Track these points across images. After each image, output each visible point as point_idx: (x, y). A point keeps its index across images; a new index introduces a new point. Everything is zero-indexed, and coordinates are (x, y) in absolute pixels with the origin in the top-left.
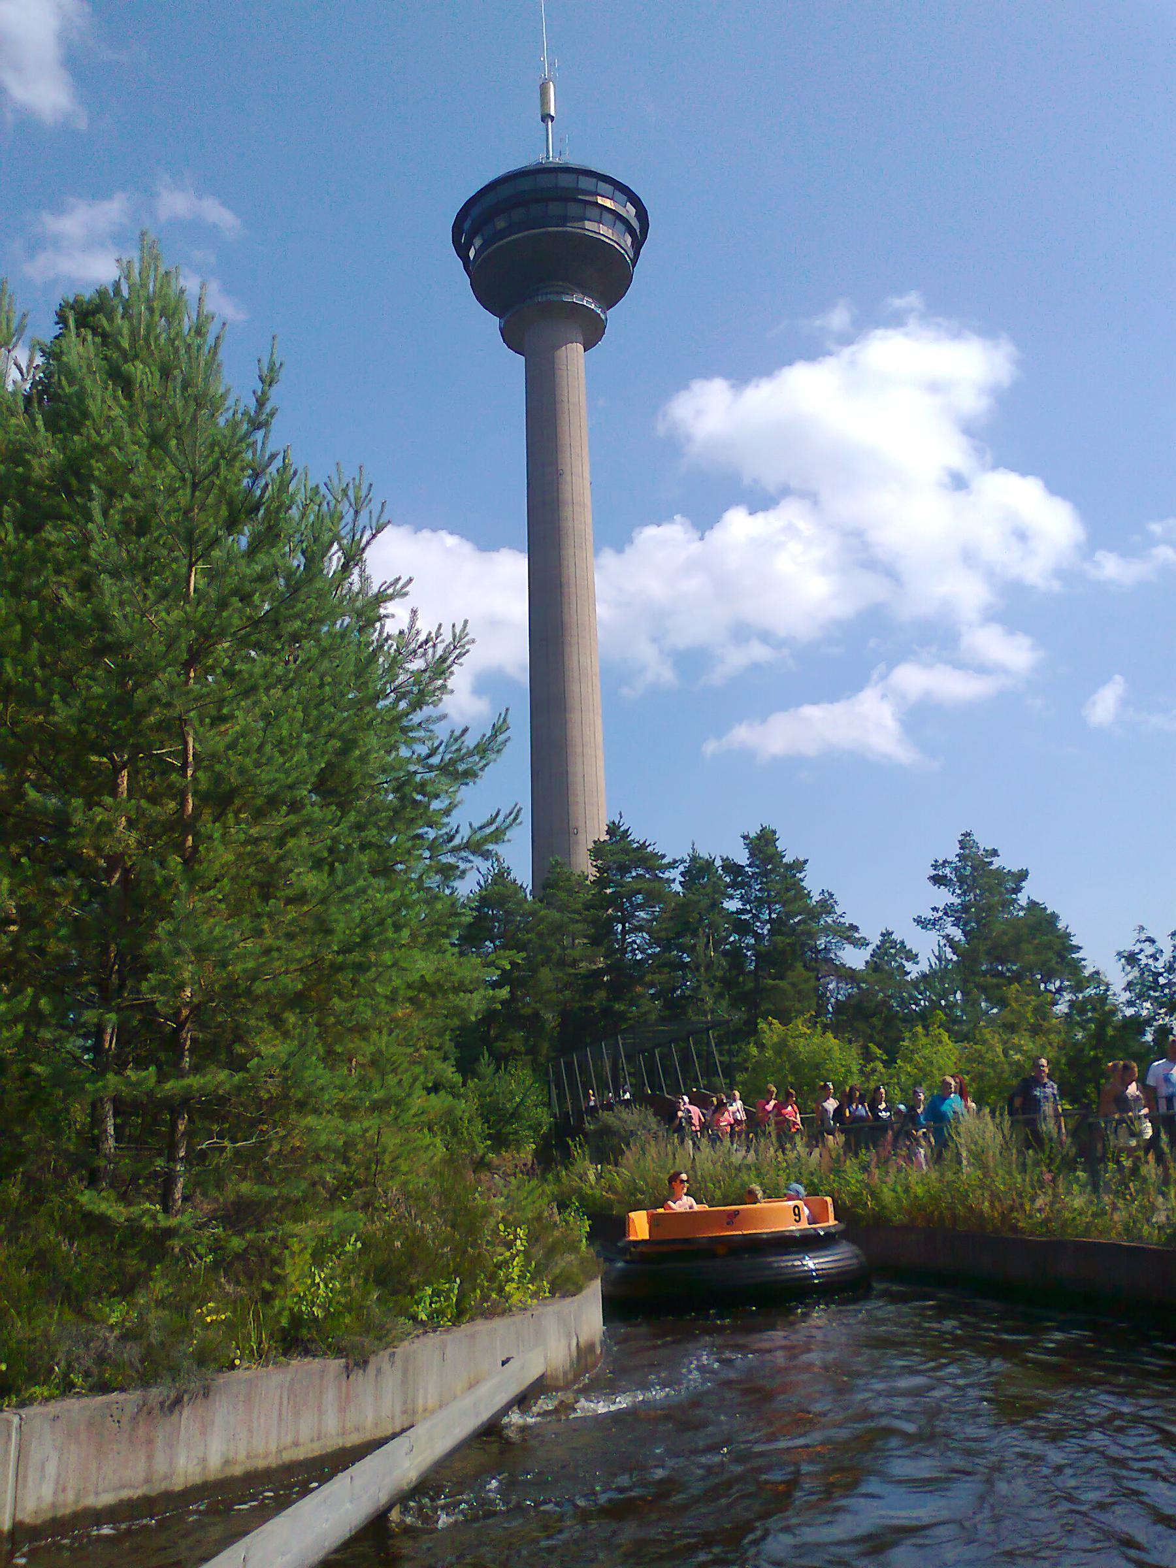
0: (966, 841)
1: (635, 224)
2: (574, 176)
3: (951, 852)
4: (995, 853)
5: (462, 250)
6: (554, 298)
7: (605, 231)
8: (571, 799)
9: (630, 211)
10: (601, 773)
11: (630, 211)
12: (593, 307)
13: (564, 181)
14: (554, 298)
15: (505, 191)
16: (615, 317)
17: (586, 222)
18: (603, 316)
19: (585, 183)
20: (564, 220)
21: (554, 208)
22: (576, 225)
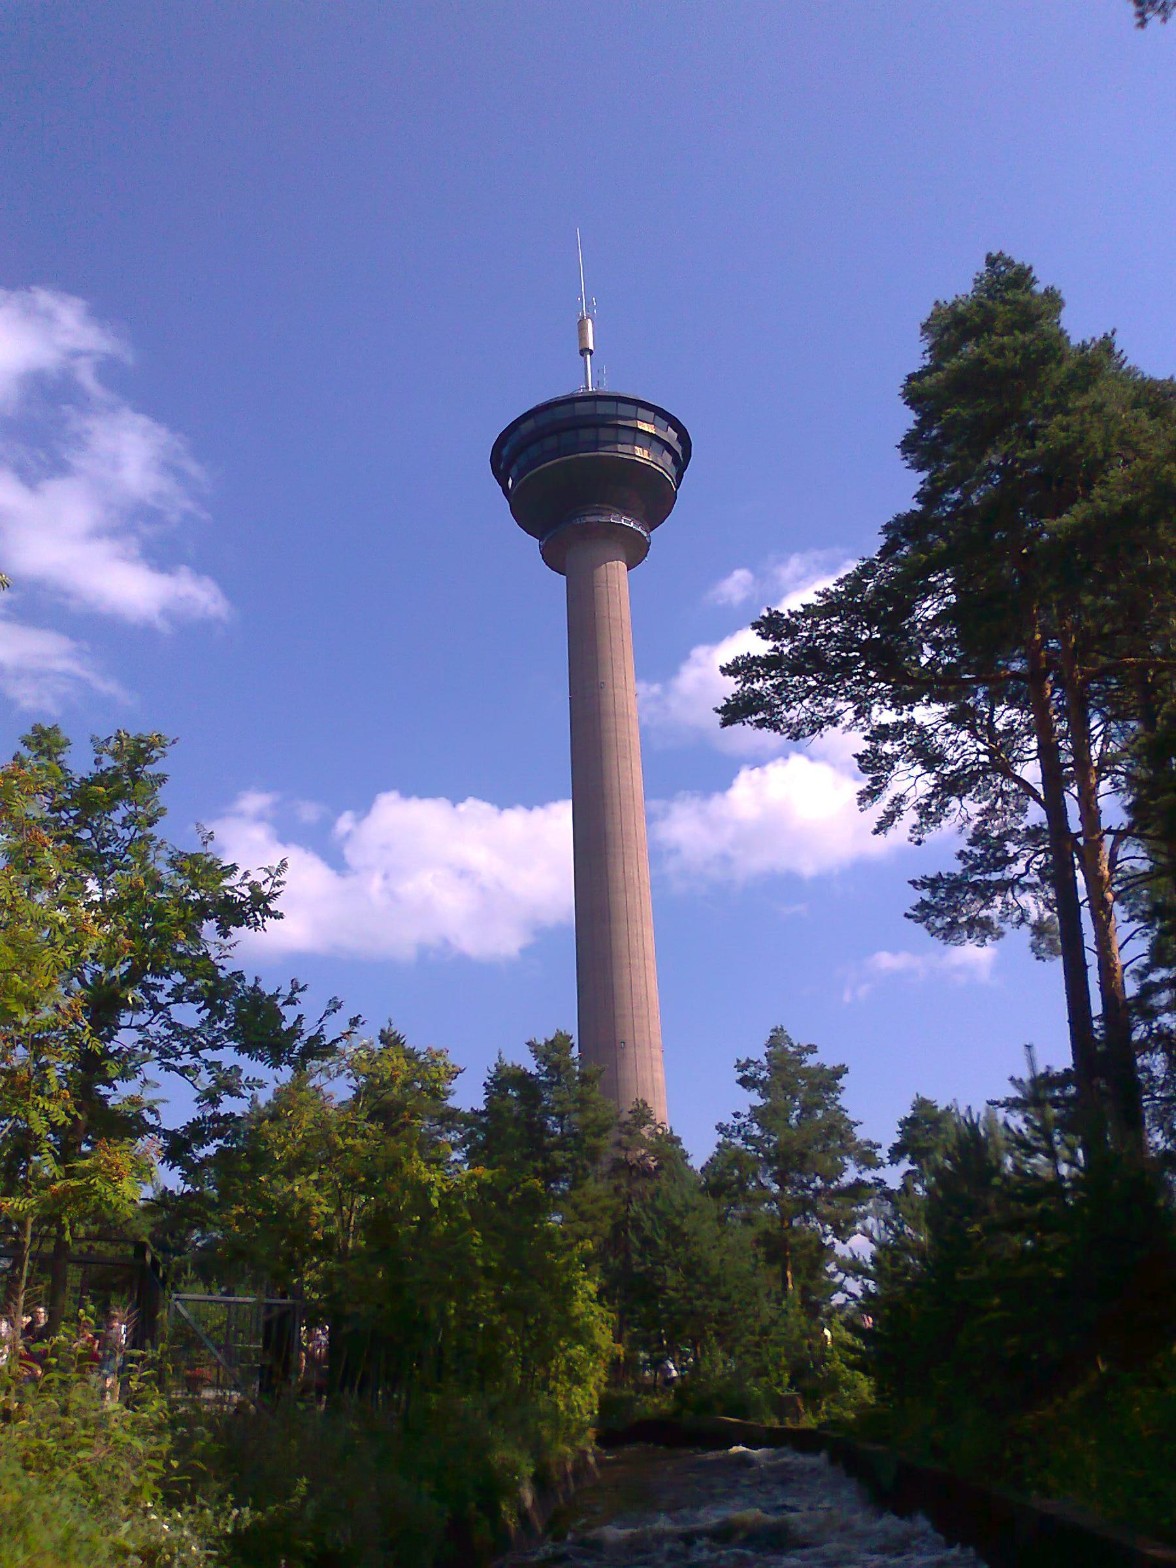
0: (777, 1038)
1: (678, 448)
2: (590, 404)
3: (758, 1052)
4: (812, 1049)
5: (501, 479)
8: (617, 1012)
9: (671, 435)
10: (653, 985)
11: (671, 435)
12: (632, 525)
13: (603, 408)
16: (657, 536)
19: (624, 409)
20: (596, 445)
21: (586, 435)
22: (608, 448)
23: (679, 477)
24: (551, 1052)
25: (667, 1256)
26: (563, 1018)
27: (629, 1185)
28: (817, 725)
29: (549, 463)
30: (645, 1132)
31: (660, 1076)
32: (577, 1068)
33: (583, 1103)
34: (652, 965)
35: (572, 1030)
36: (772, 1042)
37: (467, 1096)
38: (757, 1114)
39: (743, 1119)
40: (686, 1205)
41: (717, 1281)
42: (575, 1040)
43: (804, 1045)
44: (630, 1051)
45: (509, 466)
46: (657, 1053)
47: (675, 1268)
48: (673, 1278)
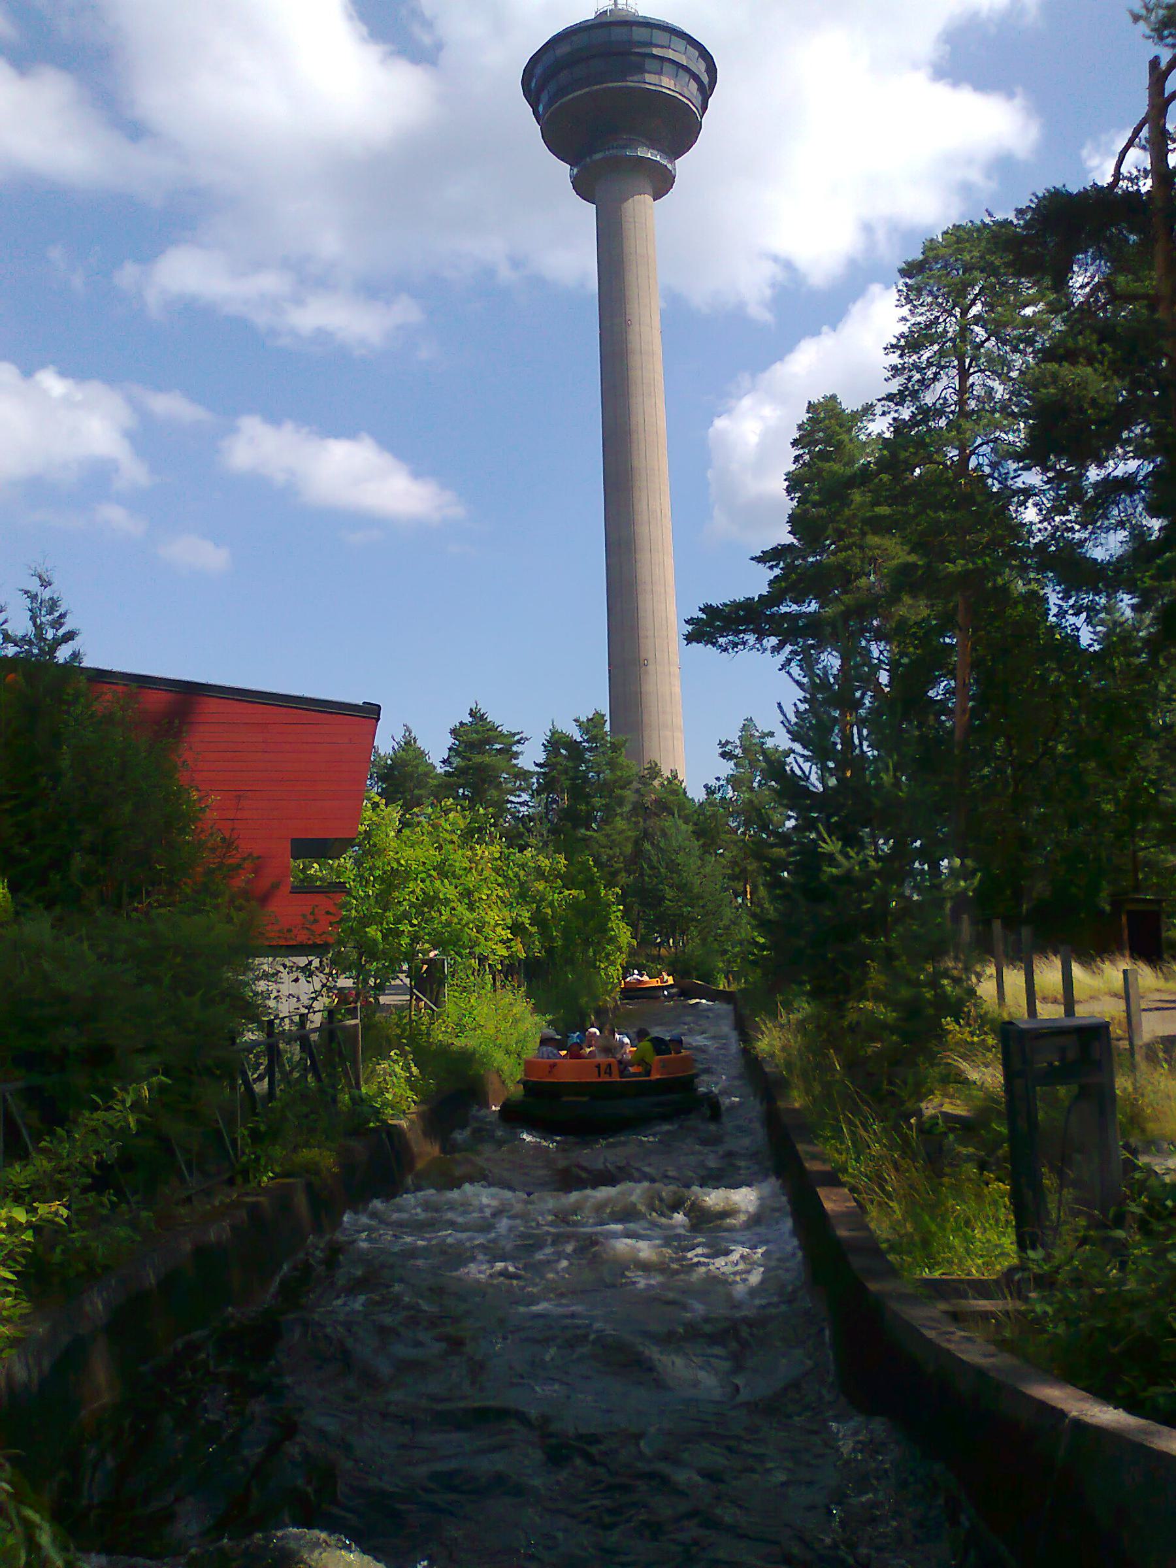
1: (705, 79)
5: (534, 103)
6: (619, 152)
7: (667, 84)
9: (700, 68)
11: (700, 68)
12: (658, 158)
14: (619, 152)
15: (563, 49)
16: (683, 166)
17: (647, 75)
18: (669, 166)
22: (635, 78)
23: (705, 108)
24: (591, 725)
25: (666, 878)
26: (596, 699)
27: (645, 820)
28: (735, 645)
29: (579, 93)
30: (656, 783)
31: (677, 690)
32: (609, 738)
33: (612, 765)
34: (671, 592)
35: (605, 710)
36: (744, 728)
37: (531, 757)
38: (730, 780)
39: (722, 782)
40: (680, 847)
41: (699, 897)
42: (607, 718)
43: (766, 731)
44: (651, 667)
45: (541, 89)
46: (675, 670)
47: (671, 887)
48: (669, 893)
